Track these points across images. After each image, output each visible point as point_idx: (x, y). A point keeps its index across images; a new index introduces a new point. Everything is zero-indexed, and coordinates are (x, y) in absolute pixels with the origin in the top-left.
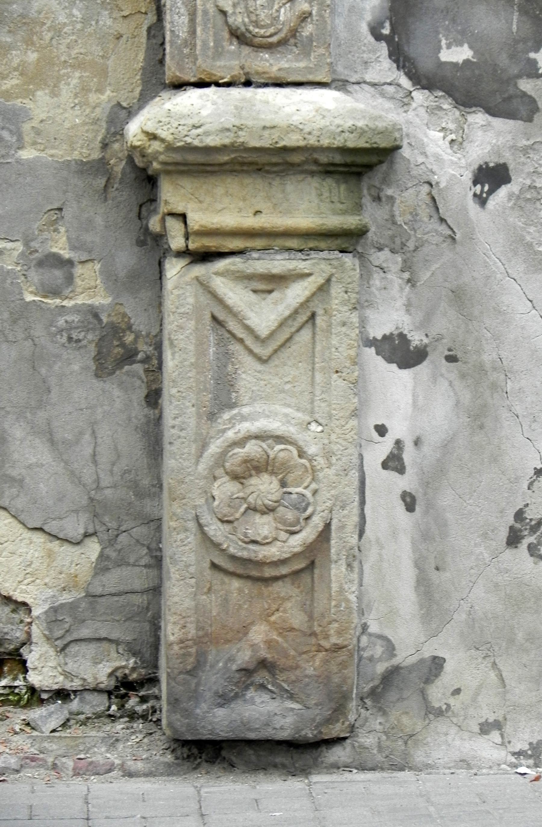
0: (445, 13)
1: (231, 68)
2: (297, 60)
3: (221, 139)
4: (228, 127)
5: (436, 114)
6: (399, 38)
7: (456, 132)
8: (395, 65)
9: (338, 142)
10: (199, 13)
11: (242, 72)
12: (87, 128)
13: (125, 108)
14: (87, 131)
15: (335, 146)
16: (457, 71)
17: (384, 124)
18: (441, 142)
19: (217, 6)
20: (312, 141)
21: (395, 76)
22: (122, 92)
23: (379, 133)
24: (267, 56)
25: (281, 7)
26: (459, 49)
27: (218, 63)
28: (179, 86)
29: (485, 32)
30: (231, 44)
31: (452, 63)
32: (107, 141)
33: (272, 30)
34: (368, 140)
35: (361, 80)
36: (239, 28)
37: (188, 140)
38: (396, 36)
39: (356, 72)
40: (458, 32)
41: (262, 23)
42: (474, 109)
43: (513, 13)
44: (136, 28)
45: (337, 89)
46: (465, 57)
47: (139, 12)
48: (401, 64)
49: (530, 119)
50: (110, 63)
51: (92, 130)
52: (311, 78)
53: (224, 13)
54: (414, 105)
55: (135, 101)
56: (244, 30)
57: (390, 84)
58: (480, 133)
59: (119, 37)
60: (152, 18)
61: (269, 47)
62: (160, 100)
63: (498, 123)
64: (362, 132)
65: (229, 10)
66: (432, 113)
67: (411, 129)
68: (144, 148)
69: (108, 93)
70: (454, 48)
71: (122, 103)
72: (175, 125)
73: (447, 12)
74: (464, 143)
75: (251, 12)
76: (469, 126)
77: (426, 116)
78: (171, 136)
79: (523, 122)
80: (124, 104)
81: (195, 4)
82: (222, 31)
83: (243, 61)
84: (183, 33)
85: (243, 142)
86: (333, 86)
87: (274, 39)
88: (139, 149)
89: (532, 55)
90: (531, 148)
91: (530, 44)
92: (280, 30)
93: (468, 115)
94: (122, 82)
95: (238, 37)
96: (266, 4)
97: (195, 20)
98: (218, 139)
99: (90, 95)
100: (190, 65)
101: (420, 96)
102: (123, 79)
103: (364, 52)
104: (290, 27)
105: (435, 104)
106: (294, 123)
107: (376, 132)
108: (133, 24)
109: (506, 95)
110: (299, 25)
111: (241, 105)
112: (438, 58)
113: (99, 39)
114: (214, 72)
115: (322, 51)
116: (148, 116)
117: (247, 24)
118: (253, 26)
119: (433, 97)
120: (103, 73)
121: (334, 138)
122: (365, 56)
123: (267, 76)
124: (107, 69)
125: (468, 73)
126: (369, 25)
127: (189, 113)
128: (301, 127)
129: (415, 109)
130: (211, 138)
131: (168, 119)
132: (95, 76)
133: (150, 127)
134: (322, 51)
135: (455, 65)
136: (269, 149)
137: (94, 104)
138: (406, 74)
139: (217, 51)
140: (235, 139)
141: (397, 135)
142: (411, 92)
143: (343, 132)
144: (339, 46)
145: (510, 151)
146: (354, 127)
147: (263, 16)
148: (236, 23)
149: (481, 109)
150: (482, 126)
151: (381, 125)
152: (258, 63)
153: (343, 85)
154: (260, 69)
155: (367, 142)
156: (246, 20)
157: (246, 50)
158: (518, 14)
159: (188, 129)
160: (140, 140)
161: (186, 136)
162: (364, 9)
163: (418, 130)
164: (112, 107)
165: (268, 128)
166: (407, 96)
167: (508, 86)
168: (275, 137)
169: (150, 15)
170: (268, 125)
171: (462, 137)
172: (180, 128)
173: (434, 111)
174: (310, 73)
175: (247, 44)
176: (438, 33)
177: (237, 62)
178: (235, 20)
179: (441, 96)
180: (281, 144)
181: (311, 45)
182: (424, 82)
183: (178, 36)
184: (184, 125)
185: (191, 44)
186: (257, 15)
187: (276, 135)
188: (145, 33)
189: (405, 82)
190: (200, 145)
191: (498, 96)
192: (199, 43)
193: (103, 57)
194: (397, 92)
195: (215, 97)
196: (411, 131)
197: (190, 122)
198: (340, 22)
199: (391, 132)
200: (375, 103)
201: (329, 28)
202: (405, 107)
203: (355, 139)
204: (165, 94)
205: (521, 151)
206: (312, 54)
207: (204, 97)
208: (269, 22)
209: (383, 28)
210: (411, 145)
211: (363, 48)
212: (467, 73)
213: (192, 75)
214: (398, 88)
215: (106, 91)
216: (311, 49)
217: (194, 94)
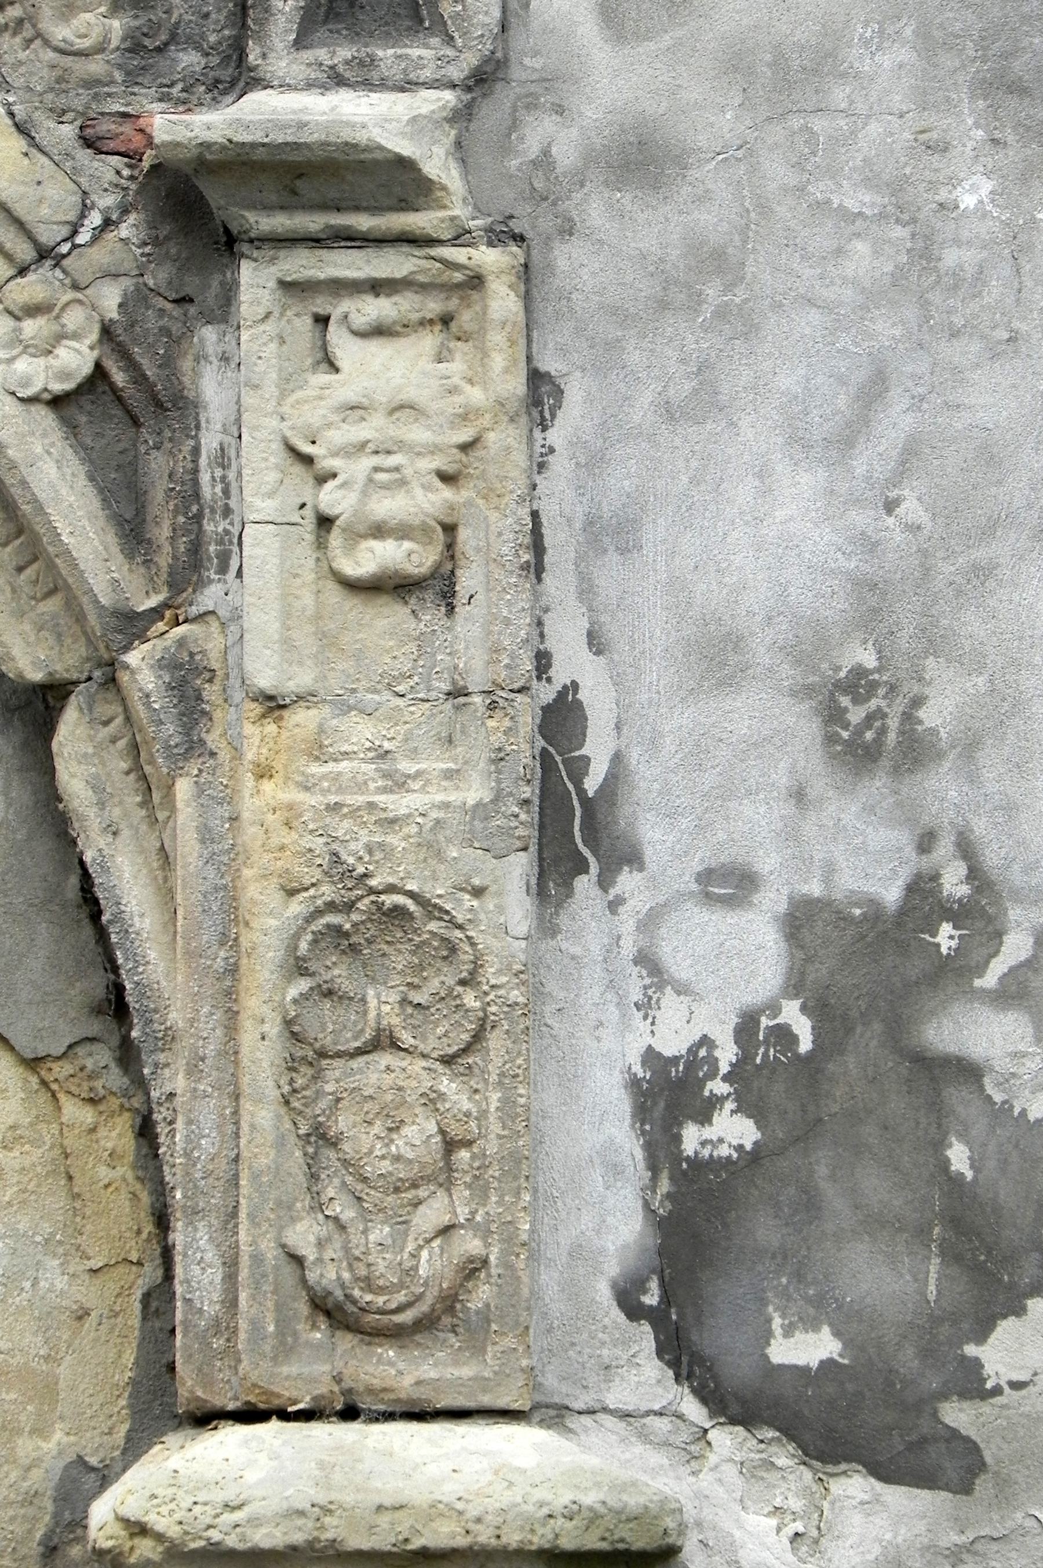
0: (779, 1260)
1: (313, 1380)
2: (456, 1363)
3: (285, 1533)
4: (300, 1507)
5: (762, 1478)
6: (678, 1315)
7: (805, 1516)
8: (671, 1373)
9: (540, 1539)
10: (245, 1261)
11: (336, 1389)
12: (11, 1512)
13: (93, 1469)
14: (13, 1519)
15: (533, 1548)
16: (806, 1386)
17: (642, 1500)
18: (773, 1537)
19: (283, 1246)
20: (484, 1537)
21: (671, 1397)
22: (88, 1435)
23: (629, 1520)
24: (391, 1353)
25: (420, 1247)
26: (811, 1337)
27: (285, 1370)
28: (205, 1419)
29: (868, 1300)
30: (314, 1327)
31: (796, 1367)
32: (56, 1540)
33: (401, 1297)
34: (607, 1535)
35: (597, 1406)
36: (330, 1293)
37: (215, 1535)
38: (673, 1310)
39: (585, 1387)
40: (809, 1300)
41: (381, 1282)
42: (843, 1466)
43: (929, 1259)
44: (118, 1295)
45: (542, 1423)
46: (824, 1355)
47: (125, 1260)
48: (684, 1372)
49: (965, 1488)
50: (63, 1371)
51: (24, 1516)
52: (486, 1400)
53: (298, 1260)
54: (713, 1458)
55: (117, 1453)
56: (342, 1298)
57: (660, 1414)
58: (857, 1518)
59: (82, 1315)
60: (151, 1273)
61: (396, 1334)
62: (162, 1450)
63: (896, 1496)
64: (594, 1517)
65: (310, 1254)
66: (753, 1476)
67: (706, 1511)
68: (121, 1554)
69: (58, 1436)
70: (799, 1336)
71: (87, 1459)
72: (186, 1503)
73: (785, 1258)
74: (823, 1540)
75: (358, 1259)
76: (833, 1503)
77: (739, 1481)
78: (178, 1528)
79: (951, 1495)
80: (93, 1461)
81: (237, 1241)
82: (295, 1299)
83: (339, 1364)
84: (210, 1304)
85: (334, 1541)
86: (537, 1417)
87: (406, 1317)
88: (109, 1557)
89: (971, 1350)
90: (968, 1551)
91: (965, 1326)
92: (419, 1298)
93: (831, 1480)
94: (89, 1413)
95: (328, 1314)
96: (390, 1241)
97: (237, 1276)
98: (278, 1534)
99: (20, 1442)
100: (226, 1374)
101: (725, 1439)
102: (91, 1405)
103: (603, 1343)
104: (441, 1290)
105: (758, 1456)
106: (445, 1499)
107: (624, 1517)
108: (113, 1288)
109: (914, 1437)
110: (461, 1285)
111: (333, 1460)
112: (766, 1358)
113: (40, 1319)
114: (276, 1389)
115: (509, 1342)
116: (129, 1486)
117: (347, 1284)
118: (362, 1289)
119: (755, 1442)
120: (47, 1391)
121: (532, 1531)
122: (605, 1352)
123: (392, 1396)
124: (56, 1383)
125: (831, 1389)
126: (614, 1285)
127: (219, 1478)
128: (460, 1506)
129: (715, 1468)
130: (264, 1530)
131: (170, 1491)
132: (31, 1400)
133: (133, 1510)
134: (509, 1342)
135: (802, 1371)
136: (390, 1554)
137: (28, 1461)
138: (695, 1391)
139: (283, 1343)
140: (316, 1533)
141: (670, 1523)
142: (706, 1431)
143: (550, 1516)
144: (550, 1330)
145: (922, 1556)
146: (575, 1507)
147: (381, 1267)
148: (324, 1281)
149: (860, 1468)
150: (862, 1503)
151: (633, 1501)
152: (371, 1369)
153: (557, 1416)
154: (376, 1383)
155: (604, 1539)
156: (346, 1275)
157: (346, 1341)
158: (938, 1261)
159: (213, 1513)
160: (112, 1538)
161: (210, 1527)
162: (602, 1251)
163: (721, 1513)
164: (66, 1468)
165: (387, 1509)
166: (699, 1439)
167: (918, 1418)
168: (404, 1529)
169: (148, 1268)
170: (387, 1502)
171: (819, 1528)
172: (197, 1509)
173: (755, 1471)
174: (485, 1391)
175: (348, 1328)
176: (764, 1302)
177: (327, 1368)
178: (322, 1275)
179: (773, 1439)
180: (416, 1544)
181: (487, 1331)
182: (735, 1409)
183: (201, 1311)
184: (206, 1504)
185: (227, 1328)
186: (369, 1265)
187: (404, 1524)
188: (137, 1306)
189: (693, 1409)
190: (240, 1546)
191: (896, 1439)
192: (243, 1325)
193: (47, 1358)
194: (676, 1431)
195: (277, 1443)
196: (707, 1514)
197: (219, 1496)
198: (550, 1280)
199: (655, 1518)
200: (628, 1455)
201: (525, 1292)
202: (693, 1463)
203: (580, 1532)
204: (172, 1439)
205: (947, 1557)
206: (489, 1349)
207: (254, 1444)
208: (395, 1281)
209: (645, 1292)
210: (706, 1545)
211: (600, 1335)
212: (830, 1390)
213: (229, 1395)
214: (678, 1421)
215: (54, 1432)
216: (486, 1339)
217: (232, 1434)
